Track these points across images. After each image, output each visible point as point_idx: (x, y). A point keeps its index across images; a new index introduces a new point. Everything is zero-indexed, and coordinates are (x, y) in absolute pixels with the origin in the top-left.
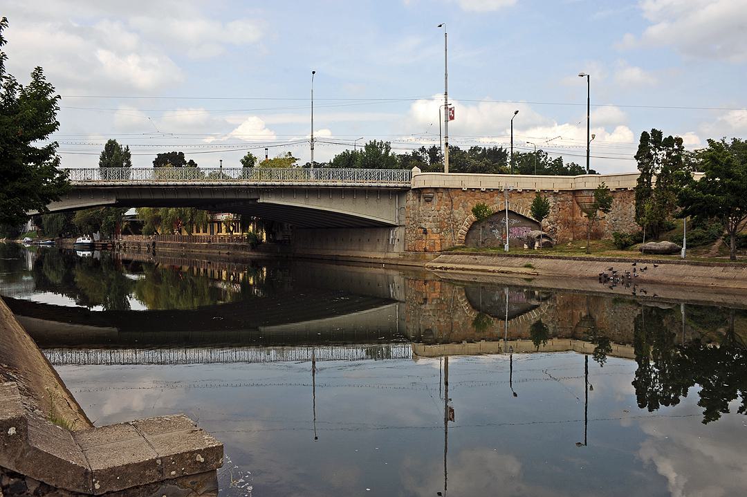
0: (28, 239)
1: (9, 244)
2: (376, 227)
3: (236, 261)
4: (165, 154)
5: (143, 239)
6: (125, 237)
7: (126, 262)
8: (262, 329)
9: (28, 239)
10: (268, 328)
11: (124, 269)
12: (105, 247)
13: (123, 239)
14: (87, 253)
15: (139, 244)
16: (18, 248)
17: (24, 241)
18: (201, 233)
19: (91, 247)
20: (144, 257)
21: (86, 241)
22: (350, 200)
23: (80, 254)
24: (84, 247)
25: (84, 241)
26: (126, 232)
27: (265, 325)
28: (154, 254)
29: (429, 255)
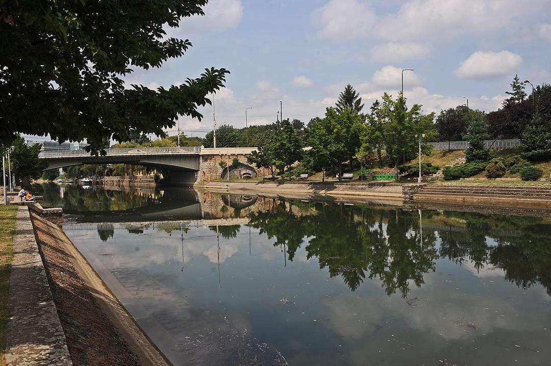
0: (60, 180)
1: (49, 183)
2: (190, 171)
3: (150, 188)
4: (173, 89)
5: (116, 179)
6: (108, 178)
7: (108, 191)
8: (143, 215)
9: (60, 180)
10: (145, 215)
11: (522, 283)
12: (97, 183)
13: (106, 179)
14: (88, 187)
15: (113, 181)
16: (54, 185)
17: (57, 181)
18: (139, 175)
19: (90, 183)
20: (116, 188)
21: (87, 180)
22: (179, 161)
23: (84, 187)
24: (86, 183)
25: (86, 180)
26: (108, 175)
27: (144, 213)
28: (119, 186)
29: (205, 182)
